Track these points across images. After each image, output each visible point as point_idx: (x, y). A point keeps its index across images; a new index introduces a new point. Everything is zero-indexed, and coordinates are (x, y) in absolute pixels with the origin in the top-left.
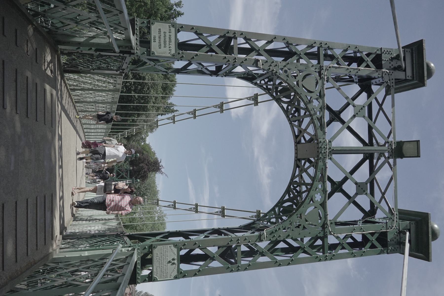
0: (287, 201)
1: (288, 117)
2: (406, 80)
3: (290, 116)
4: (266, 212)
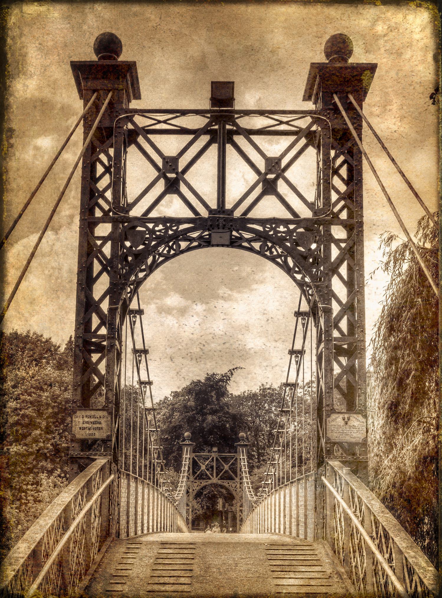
0: (286, 262)
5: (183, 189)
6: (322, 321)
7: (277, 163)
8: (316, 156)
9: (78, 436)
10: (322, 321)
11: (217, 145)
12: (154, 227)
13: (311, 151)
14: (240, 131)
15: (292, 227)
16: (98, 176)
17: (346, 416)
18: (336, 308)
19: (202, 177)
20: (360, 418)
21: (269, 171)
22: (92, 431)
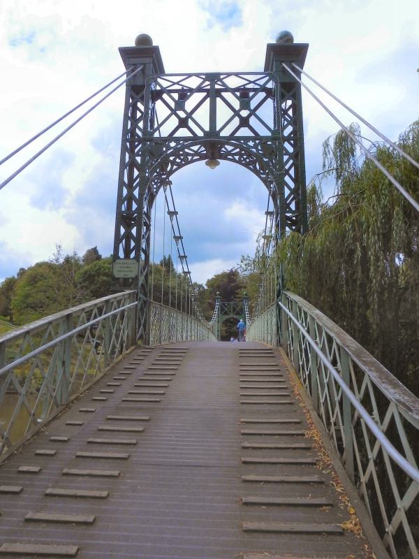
0: (255, 167)
2: (153, 63)
3: (183, 163)
5: (191, 123)
13: (270, 102)
14: (227, 89)
22: (125, 273)
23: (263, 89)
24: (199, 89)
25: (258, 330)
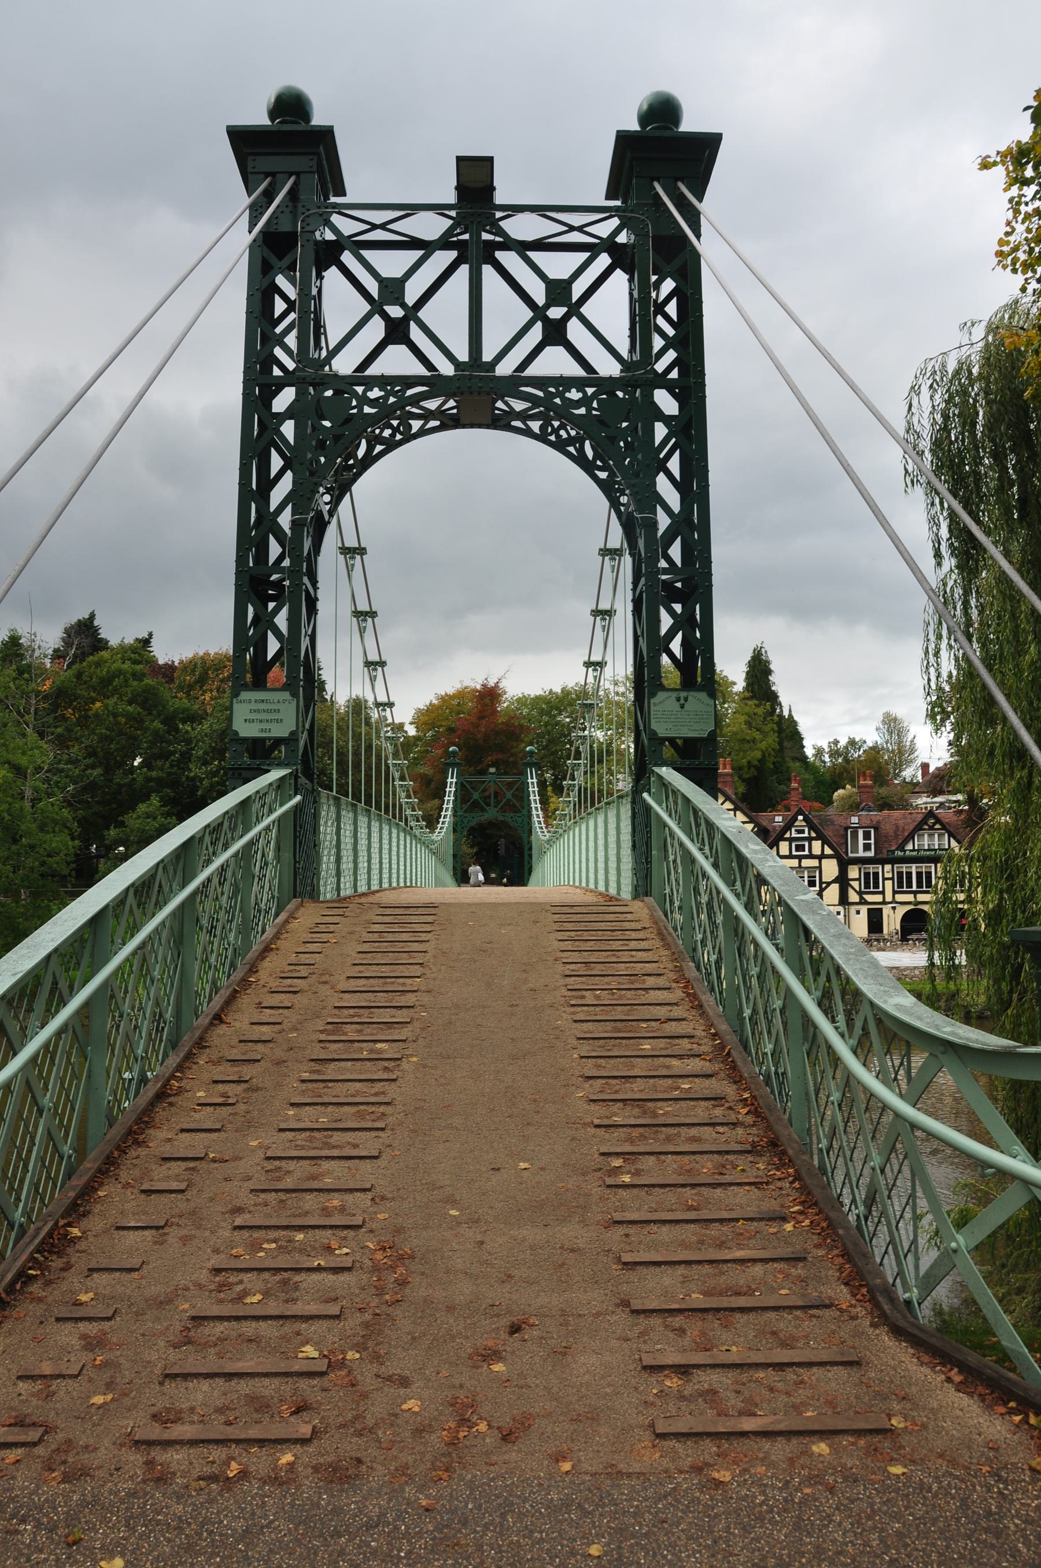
0: (581, 451)
1: (401, 443)
4: (608, 504)
5: (416, 334)
6: (641, 543)
7: (564, 288)
8: (627, 284)
9: (243, 734)
10: (641, 543)
11: (467, 266)
12: (365, 392)
13: (620, 277)
14: (509, 244)
15: (590, 391)
16: (276, 316)
17: (683, 694)
18: (663, 521)
19: (446, 315)
20: (703, 696)
21: (552, 300)
23: (609, 245)
24: (444, 243)
25: (580, 857)
